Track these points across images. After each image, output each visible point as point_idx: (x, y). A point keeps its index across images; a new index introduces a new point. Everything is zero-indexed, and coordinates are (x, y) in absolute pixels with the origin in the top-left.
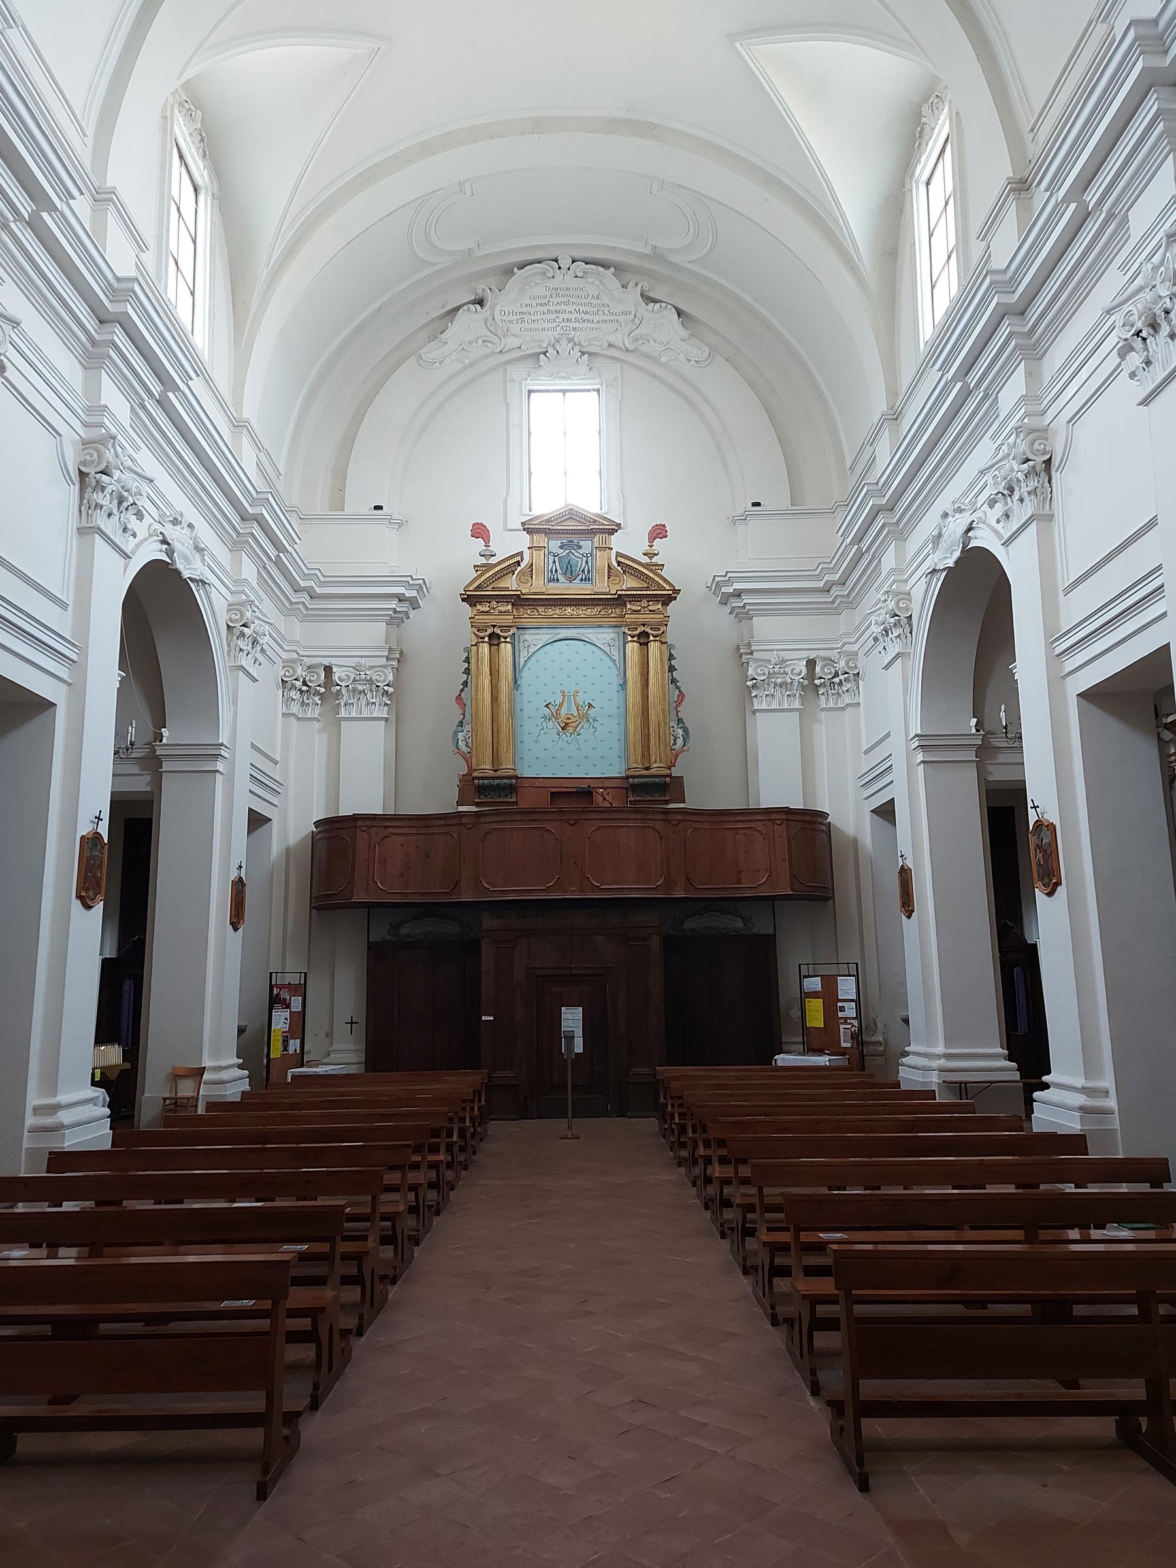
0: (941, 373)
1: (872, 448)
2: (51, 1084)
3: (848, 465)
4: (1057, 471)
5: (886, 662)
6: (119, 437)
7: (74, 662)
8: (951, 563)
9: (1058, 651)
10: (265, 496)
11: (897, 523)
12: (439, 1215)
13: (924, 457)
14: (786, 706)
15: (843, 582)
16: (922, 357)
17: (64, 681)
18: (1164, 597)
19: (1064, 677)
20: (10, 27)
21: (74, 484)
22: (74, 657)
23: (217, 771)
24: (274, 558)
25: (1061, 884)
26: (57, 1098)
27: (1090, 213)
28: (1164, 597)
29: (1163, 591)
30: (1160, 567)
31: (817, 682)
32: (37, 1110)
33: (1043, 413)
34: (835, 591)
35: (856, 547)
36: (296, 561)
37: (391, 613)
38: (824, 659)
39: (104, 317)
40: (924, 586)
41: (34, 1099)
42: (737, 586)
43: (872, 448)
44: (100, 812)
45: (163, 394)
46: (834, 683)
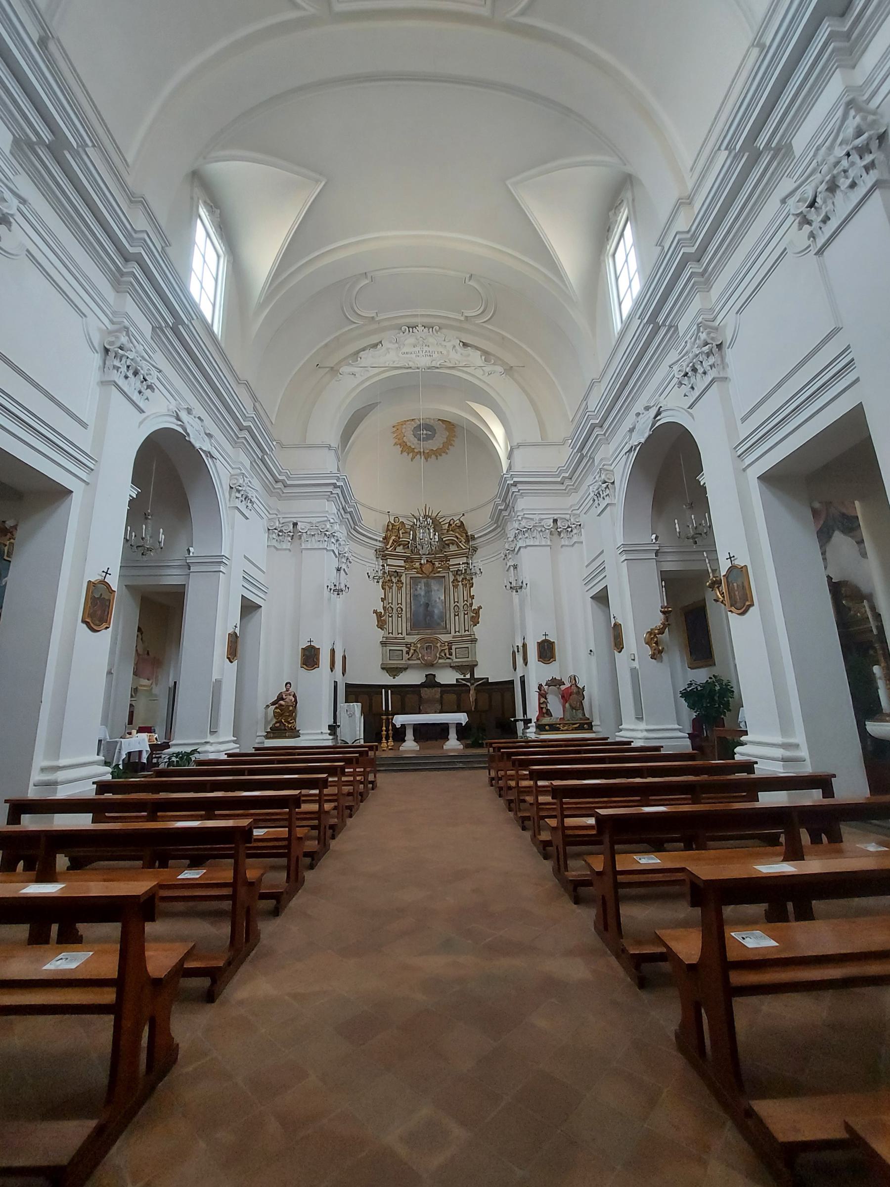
0: (640, 320)
1: (585, 402)
2: (55, 748)
3: (571, 420)
4: (728, 348)
5: (599, 512)
6: (131, 328)
7: (92, 470)
8: (643, 440)
9: (739, 453)
10: (252, 415)
11: (604, 434)
12: (334, 839)
13: (618, 395)
14: (544, 544)
15: (570, 477)
16: (616, 339)
17: (84, 481)
18: (855, 367)
19: (744, 470)
20: (167, 246)
21: (97, 352)
22: (92, 466)
23: (221, 571)
24: (171, 324)
25: (753, 605)
26: (60, 761)
27: (762, 152)
28: (855, 367)
29: (854, 364)
30: (848, 347)
31: (559, 530)
32: (43, 770)
33: (716, 317)
34: (567, 482)
35: (580, 454)
36: (203, 349)
37: (329, 494)
38: (562, 519)
39: (277, 480)
40: (625, 460)
41: (40, 760)
42: (515, 479)
43: (585, 402)
44: (108, 569)
45: (263, 456)
46: (569, 530)
